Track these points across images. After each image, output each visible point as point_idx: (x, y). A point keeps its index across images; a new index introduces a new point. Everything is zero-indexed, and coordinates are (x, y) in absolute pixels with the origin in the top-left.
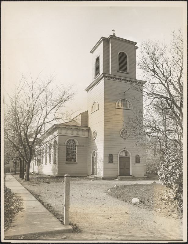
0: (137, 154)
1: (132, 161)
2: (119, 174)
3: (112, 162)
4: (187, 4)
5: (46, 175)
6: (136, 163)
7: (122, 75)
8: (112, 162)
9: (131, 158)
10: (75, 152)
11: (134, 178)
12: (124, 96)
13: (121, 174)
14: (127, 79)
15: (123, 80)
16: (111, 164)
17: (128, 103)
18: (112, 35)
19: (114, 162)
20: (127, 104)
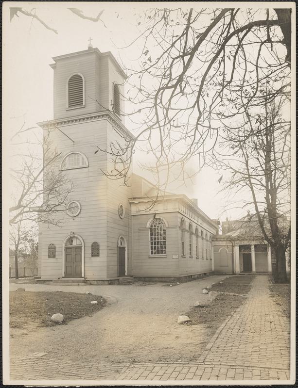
0: (95, 241)
1: (87, 252)
2: (63, 275)
3: (54, 256)
4: (280, 29)
5: (148, 284)
6: (92, 256)
7: (77, 112)
8: (54, 256)
9: (126, 249)
10: (152, 243)
11: (86, 282)
12: (73, 148)
13: (67, 275)
14: (70, 119)
15: (87, 118)
16: (52, 260)
17: (80, 157)
18: (87, 49)
19: (57, 257)
20: (78, 159)
